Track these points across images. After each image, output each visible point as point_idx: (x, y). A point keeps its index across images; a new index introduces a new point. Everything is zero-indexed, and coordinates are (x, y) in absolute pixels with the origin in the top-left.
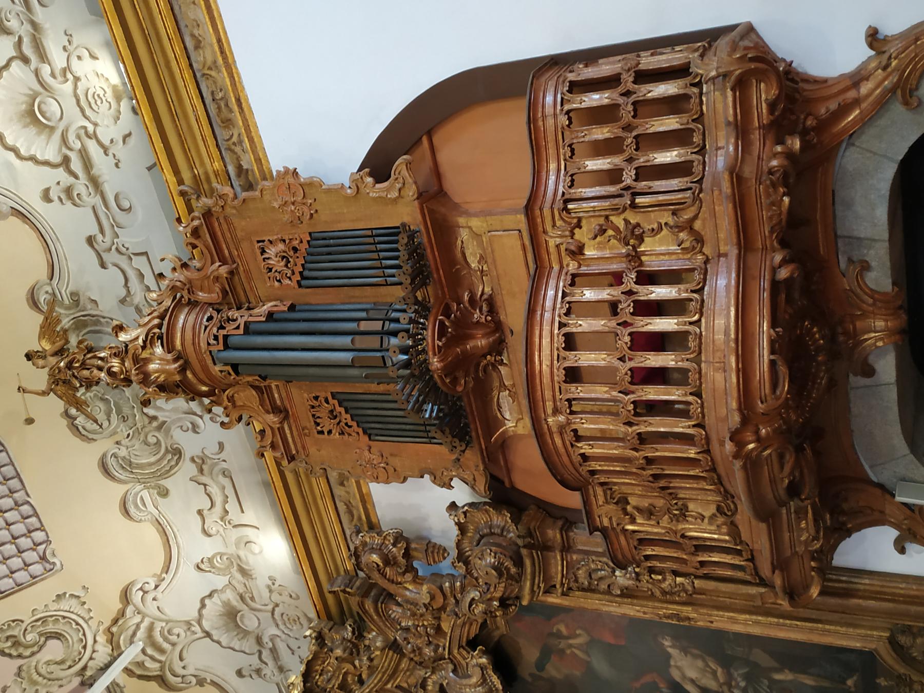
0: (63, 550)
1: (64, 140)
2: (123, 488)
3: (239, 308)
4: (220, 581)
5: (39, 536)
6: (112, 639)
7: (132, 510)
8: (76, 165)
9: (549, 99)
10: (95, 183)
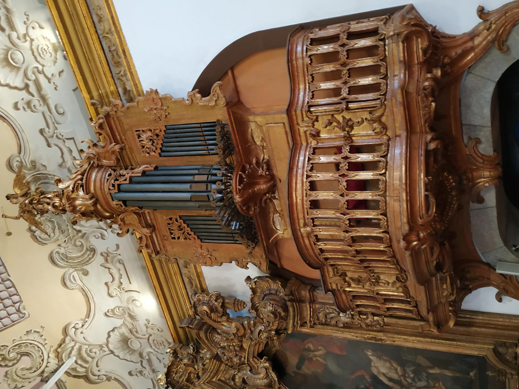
0: (29, 305)
1: (25, 75)
2: (63, 271)
3: (126, 169)
4: (118, 322)
5: (16, 298)
6: (58, 355)
7: (68, 283)
8: (33, 89)
9: (299, 49)
10: (44, 99)
